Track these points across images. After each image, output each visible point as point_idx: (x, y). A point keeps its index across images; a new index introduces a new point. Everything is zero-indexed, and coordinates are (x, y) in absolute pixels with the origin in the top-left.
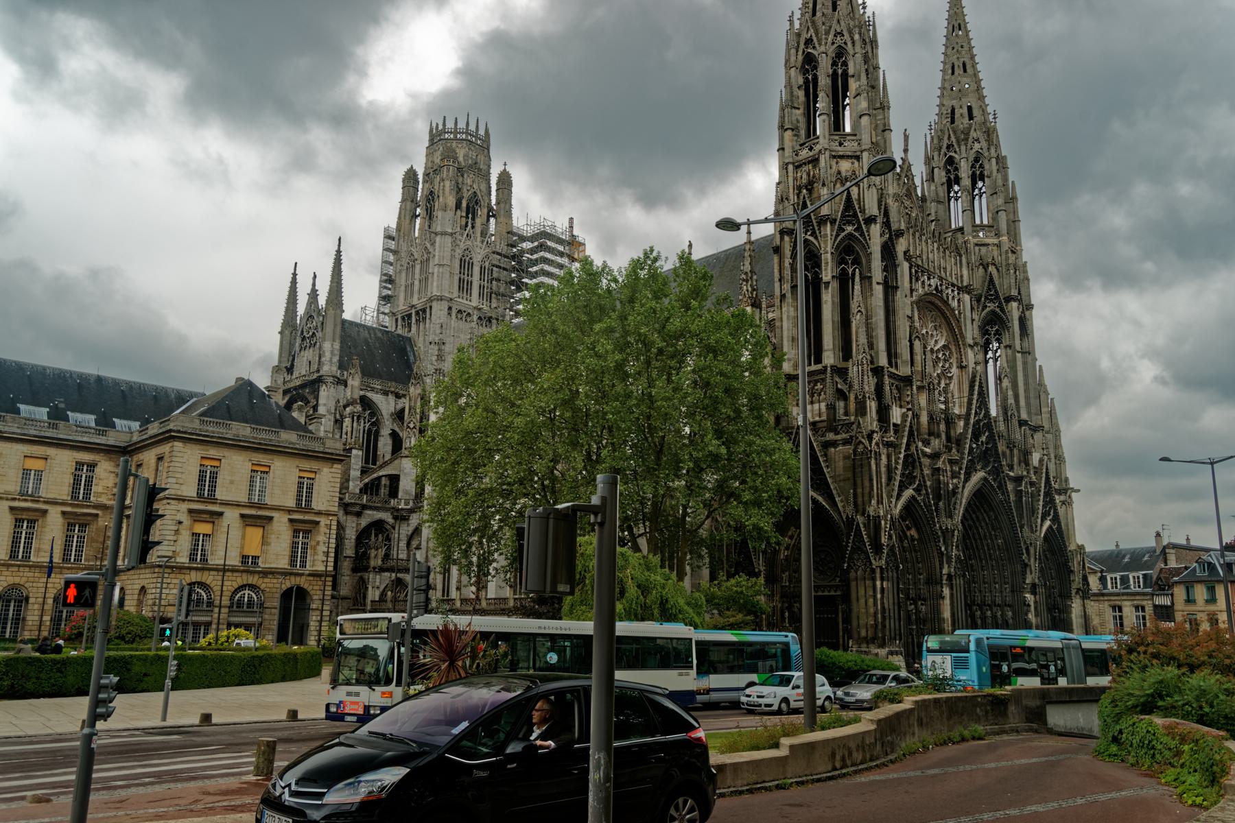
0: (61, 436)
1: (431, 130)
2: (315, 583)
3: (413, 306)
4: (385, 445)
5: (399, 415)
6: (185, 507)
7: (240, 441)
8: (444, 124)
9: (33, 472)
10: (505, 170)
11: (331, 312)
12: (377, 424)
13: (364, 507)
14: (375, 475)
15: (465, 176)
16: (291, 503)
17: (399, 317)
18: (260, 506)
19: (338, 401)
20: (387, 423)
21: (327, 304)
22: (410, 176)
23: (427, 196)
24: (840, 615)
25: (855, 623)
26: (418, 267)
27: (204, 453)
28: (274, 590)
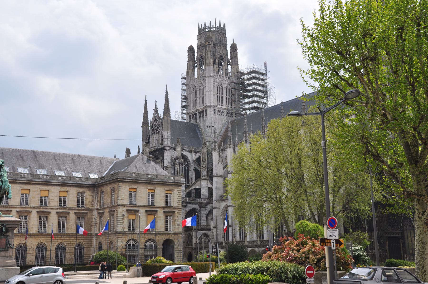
0: (72, 182)
1: (199, 27)
2: (175, 237)
3: (197, 110)
4: (192, 175)
5: (198, 161)
6: (125, 209)
7: (143, 180)
8: (205, 25)
9: (63, 197)
10: (234, 43)
11: (166, 118)
12: (188, 166)
13: (187, 203)
14: (190, 189)
15: (216, 48)
16: (163, 204)
17: (191, 115)
18: (153, 206)
19: (172, 157)
20: (192, 165)
21: (164, 115)
22: (191, 49)
23: (199, 58)
24: (401, 244)
25: (407, 248)
26: (198, 92)
27: (130, 187)
28: (160, 241)
